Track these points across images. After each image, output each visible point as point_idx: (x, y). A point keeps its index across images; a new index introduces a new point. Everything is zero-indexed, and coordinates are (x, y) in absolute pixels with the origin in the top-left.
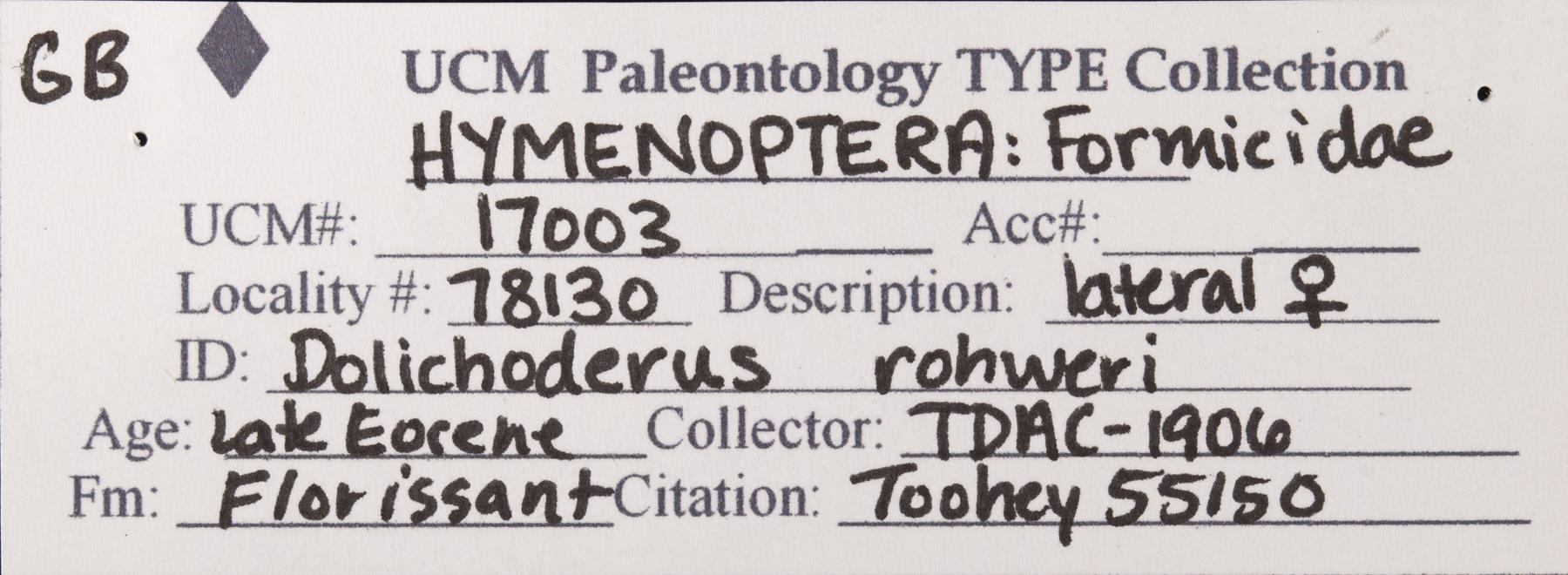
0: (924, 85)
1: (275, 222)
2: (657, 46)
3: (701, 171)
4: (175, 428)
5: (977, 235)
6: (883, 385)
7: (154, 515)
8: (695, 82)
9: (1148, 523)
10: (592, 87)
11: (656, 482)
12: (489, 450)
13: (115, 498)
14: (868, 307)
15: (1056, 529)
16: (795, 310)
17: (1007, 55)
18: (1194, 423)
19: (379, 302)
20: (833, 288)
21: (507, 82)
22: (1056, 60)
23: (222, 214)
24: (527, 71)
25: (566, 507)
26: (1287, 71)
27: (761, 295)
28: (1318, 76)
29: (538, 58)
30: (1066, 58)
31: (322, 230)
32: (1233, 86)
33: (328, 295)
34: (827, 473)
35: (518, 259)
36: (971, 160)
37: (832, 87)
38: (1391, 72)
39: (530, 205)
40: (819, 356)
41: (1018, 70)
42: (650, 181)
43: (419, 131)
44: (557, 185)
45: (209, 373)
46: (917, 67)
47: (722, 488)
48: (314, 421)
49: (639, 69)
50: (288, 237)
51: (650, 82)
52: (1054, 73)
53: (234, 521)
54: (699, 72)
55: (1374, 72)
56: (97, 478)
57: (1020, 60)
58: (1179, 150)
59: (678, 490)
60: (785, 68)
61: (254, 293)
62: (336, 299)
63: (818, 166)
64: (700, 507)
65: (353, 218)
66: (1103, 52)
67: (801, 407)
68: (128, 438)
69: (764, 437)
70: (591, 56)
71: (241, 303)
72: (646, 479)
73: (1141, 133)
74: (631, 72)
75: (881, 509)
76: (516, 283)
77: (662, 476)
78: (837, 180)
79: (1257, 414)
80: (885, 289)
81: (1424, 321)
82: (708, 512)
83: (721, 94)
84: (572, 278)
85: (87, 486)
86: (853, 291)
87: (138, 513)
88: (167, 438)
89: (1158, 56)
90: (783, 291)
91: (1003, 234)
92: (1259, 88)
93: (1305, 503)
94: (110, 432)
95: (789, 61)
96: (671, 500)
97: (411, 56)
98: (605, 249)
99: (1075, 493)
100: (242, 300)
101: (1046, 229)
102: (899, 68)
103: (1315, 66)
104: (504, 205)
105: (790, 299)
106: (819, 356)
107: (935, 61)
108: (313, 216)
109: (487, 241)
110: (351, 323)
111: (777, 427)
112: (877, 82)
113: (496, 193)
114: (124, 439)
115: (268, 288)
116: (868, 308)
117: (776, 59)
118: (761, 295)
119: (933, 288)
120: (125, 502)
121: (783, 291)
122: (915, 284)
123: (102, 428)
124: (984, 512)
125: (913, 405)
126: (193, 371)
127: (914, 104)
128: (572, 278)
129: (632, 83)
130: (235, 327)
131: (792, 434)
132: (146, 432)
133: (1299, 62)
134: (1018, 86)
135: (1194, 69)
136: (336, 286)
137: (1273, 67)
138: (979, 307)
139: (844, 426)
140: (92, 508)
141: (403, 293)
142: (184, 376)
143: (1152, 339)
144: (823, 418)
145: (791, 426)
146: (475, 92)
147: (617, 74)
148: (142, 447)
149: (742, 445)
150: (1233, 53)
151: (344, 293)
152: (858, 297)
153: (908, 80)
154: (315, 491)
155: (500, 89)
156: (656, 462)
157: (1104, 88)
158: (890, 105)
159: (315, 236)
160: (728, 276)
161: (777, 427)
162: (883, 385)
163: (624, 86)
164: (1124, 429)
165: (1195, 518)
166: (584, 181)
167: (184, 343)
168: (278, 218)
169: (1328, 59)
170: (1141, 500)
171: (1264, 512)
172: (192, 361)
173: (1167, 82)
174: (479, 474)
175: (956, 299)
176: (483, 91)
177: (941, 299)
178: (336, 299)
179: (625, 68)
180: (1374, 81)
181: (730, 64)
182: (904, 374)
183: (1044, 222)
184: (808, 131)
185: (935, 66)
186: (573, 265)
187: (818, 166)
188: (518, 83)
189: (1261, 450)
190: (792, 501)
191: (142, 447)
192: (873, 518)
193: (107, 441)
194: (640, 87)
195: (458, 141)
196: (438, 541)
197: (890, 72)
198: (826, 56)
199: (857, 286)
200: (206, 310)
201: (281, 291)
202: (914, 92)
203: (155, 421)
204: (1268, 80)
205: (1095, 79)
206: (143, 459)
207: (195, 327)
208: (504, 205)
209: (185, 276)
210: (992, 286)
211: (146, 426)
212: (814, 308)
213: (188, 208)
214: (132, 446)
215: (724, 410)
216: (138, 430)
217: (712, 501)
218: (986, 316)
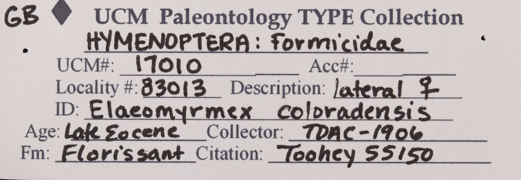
0: (286, 22)
4: (54, 131)
8: (201, 20)
10: (163, 22)
11: (210, 149)
13: (35, 153)
16: (255, 93)
17: (316, 11)
19: (121, 89)
20: (267, 86)
22: (335, 13)
24: (140, 16)
26: (419, 18)
27: (244, 88)
28: (430, 19)
29: (144, 11)
31: (103, 67)
32: (399, 23)
33: (105, 88)
34: (268, 148)
37: (252, 22)
38: (457, 18)
39: (154, 58)
40: (265, 107)
41: (320, 17)
44: (205, 54)
46: (283, 15)
47: (231, 151)
48: (96, 129)
49: (180, 15)
50: (92, 69)
51: (184, 20)
54: (203, 17)
56: (30, 147)
57: (321, 13)
59: (217, 151)
60: (235, 15)
63: (200, 47)
64: (224, 157)
66: (352, 11)
67: (256, 125)
69: (245, 134)
70: (163, 11)
71: (76, 90)
74: (177, 16)
78: (272, 53)
80: (284, 86)
82: (226, 159)
84: (194, 82)
85: (26, 149)
87: (43, 158)
88: (52, 134)
89: (372, 12)
90: (251, 87)
91: (322, 69)
93: (426, 156)
95: (236, 13)
96: (215, 155)
97: (98, 11)
99: (353, 152)
100: (77, 89)
101: (336, 68)
102: (277, 16)
105: (253, 90)
106: (265, 107)
109: (139, 69)
110: (112, 97)
114: (38, 134)
116: (278, 93)
117: (231, 12)
118: (244, 88)
120: (39, 154)
121: (251, 87)
122: (294, 85)
125: (305, 125)
126: (61, 112)
127: (282, 29)
128: (194, 82)
129: (178, 21)
131: (254, 133)
133: (424, 14)
134: (320, 22)
136: (107, 85)
137: (414, 16)
140: (28, 156)
142: (58, 114)
144: (264, 128)
146: (122, 23)
147: (173, 17)
149: (237, 137)
150: (399, 11)
151: (110, 88)
152: (275, 89)
153: (280, 20)
154: (95, 152)
155: (130, 23)
156: (210, 142)
157: (352, 23)
159: (100, 69)
161: (249, 131)
163: (175, 22)
164: (367, 132)
167: (58, 103)
169: (434, 13)
172: (60, 109)
176: (124, 23)
177: (301, 90)
179: (175, 15)
183: (335, 66)
184: (197, 38)
185: (290, 15)
186: (195, 78)
187: (200, 47)
188: (136, 21)
190: (254, 155)
194: (181, 22)
197: (274, 17)
198: (249, 11)
199: (275, 86)
200: (65, 93)
201: (89, 86)
202: (282, 24)
204: (412, 21)
205: (349, 20)
206: (44, 140)
207: (62, 98)
208: (146, 59)
209: (58, 81)
210: (318, 86)
211: (45, 130)
213: (59, 60)
214: (41, 136)
215: (232, 126)
216: (43, 131)
217: (227, 155)
218: (317, 96)
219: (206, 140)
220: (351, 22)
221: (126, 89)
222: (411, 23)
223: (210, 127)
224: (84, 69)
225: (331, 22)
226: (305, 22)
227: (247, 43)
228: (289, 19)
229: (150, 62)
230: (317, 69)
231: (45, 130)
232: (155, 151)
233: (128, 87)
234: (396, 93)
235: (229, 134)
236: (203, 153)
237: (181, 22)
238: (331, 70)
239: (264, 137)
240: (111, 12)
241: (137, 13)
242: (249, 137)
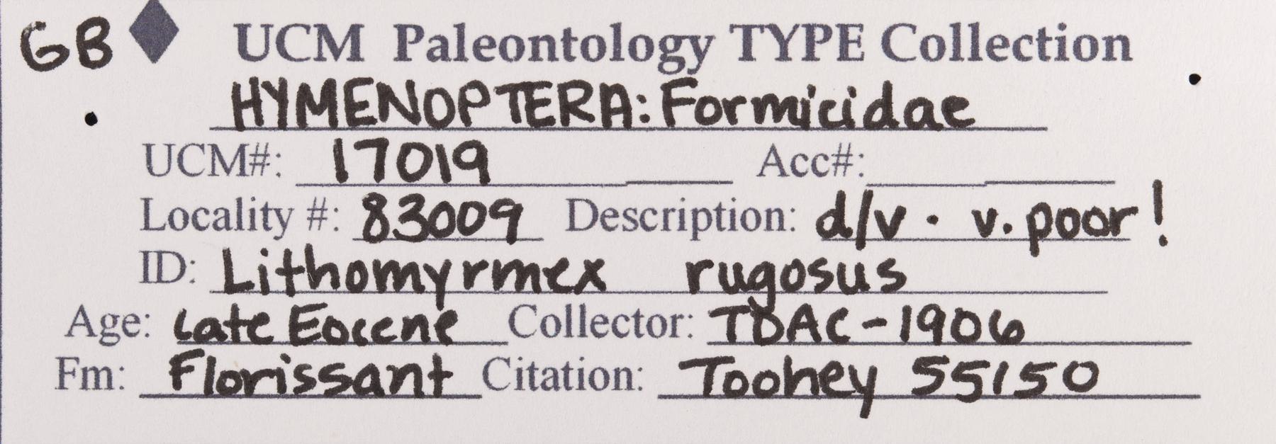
0: (700, 55)
3: (423, 123)
5: (768, 170)
6: (694, 287)
8: (495, 52)
10: (402, 56)
11: (515, 364)
13: (91, 375)
16: (625, 229)
17: (774, 29)
18: (940, 316)
19: (298, 221)
20: (655, 212)
22: (819, 34)
24: (344, 43)
25: (428, 386)
28: (1052, 48)
29: (355, 31)
30: (828, 31)
32: (975, 57)
36: (617, 120)
37: (617, 57)
38: (1118, 46)
40: (644, 266)
41: (783, 43)
43: (237, 88)
46: (694, 40)
47: (567, 369)
50: (228, 171)
51: (453, 52)
55: (528, 46)
56: (77, 359)
58: (769, 111)
59: (532, 369)
60: (576, 39)
61: (201, 214)
62: (265, 220)
63: (516, 118)
64: (550, 383)
66: (861, 27)
67: (628, 305)
69: (600, 329)
70: (402, 29)
72: (507, 361)
73: (741, 100)
77: (520, 359)
79: (996, 315)
80: (695, 212)
81: (653, 293)
82: (556, 388)
85: (69, 366)
88: (131, 328)
89: (910, 30)
91: (788, 169)
94: (87, 324)
95: (579, 33)
96: (527, 378)
97: (242, 29)
99: (873, 372)
100: (191, 219)
101: (822, 166)
102: (678, 40)
103: (1050, 39)
105: (621, 221)
106: (644, 266)
110: (276, 238)
114: (97, 328)
115: (211, 212)
116: (682, 228)
117: (567, 32)
119: (733, 212)
122: (719, 210)
123: (81, 320)
126: (153, 275)
127: (690, 72)
129: (437, 53)
131: (623, 326)
132: (115, 323)
133: (1035, 36)
134: (784, 56)
135: (601, 41)
140: (73, 383)
141: (317, 214)
142: (146, 279)
144: (647, 314)
145: (621, 320)
146: (301, 60)
147: (424, 45)
148: (112, 335)
149: (583, 334)
150: (975, 28)
151: (272, 216)
152: (674, 219)
153: (686, 50)
155: (320, 58)
156: (516, 347)
159: (248, 169)
160: (572, 202)
161: (611, 321)
162: (694, 287)
163: (431, 56)
164: (881, 322)
167: (146, 254)
168: (219, 153)
169: (1060, 34)
170: (1043, 383)
172: (152, 269)
174: (400, 355)
177: (739, 221)
178: (265, 220)
179: (430, 40)
180: (528, 52)
182: (709, 279)
183: (820, 160)
185: (710, 38)
188: (336, 53)
189: (1003, 340)
190: (621, 379)
191: (112, 335)
193: (84, 330)
194: (445, 57)
195: (264, 94)
197: (670, 44)
199: (673, 210)
200: (163, 228)
201: (222, 213)
202: (691, 61)
203: (122, 312)
205: (853, 51)
206: (113, 344)
207: (154, 241)
208: (360, 145)
209: (147, 201)
210: (779, 211)
211: (115, 318)
213: (149, 147)
215: (569, 308)
216: (109, 321)
217: (559, 379)
219: (505, 343)
220: (859, 56)
221: (311, 219)
223: (516, 309)
225: (810, 56)
226: (747, 56)
228: (708, 46)
229: (372, 152)
231: (115, 318)
232: (371, 370)
233: (317, 214)
235: (562, 326)
236: (501, 374)
237: (445, 57)
238: (810, 172)
239: (647, 335)
240: (274, 34)
241: (339, 35)
242: (611, 334)
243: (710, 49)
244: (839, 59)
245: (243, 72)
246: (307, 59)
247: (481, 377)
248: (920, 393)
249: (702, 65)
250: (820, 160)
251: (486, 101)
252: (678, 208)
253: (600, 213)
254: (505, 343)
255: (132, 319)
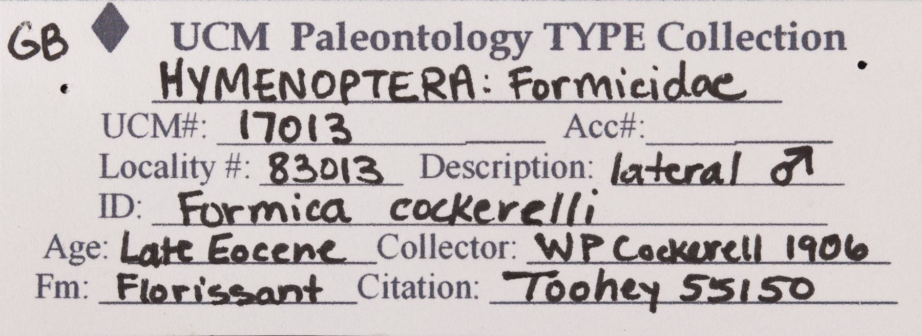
0: (522, 46)
1: (157, 124)
2: (341, 20)
4: (98, 246)
7: (86, 297)
8: (367, 43)
9: (735, 303)
10: (298, 46)
11: (382, 279)
12: (292, 260)
13: (63, 287)
14: (508, 175)
15: (648, 306)
16: (465, 177)
19: (219, 171)
20: (487, 164)
21: (241, 44)
22: (611, 30)
23: (126, 120)
24: (254, 37)
27: (444, 168)
28: (786, 41)
31: (185, 129)
32: (728, 47)
33: (189, 167)
35: (284, 146)
36: (462, 90)
37: (459, 47)
38: (835, 39)
42: (379, 102)
45: (119, 213)
46: (517, 35)
47: (421, 282)
49: (329, 35)
50: (166, 134)
51: (336, 44)
52: (609, 40)
53: (318, 300)
56: (52, 276)
57: (586, 30)
59: (395, 282)
60: (428, 34)
61: (145, 166)
64: (408, 293)
65: (642, 122)
66: (642, 25)
68: (71, 252)
69: (446, 252)
70: (297, 26)
71: (137, 172)
72: (377, 276)
74: (324, 37)
75: (529, 296)
76: (278, 160)
78: (313, 102)
80: (518, 164)
82: (413, 296)
83: (445, 51)
86: (499, 166)
87: (76, 296)
88: (94, 252)
89: (679, 27)
91: (587, 132)
92: (362, 49)
95: (431, 29)
96: (391, 289)
97: (177, 27)
98: (290, 141)
100: (137, 170)
101: (612, 129)
102: (505, 34)
103: (784, 33)
104: (257, 115)
105: (462, 170)
107: (528, 30)
108: (180, 121)
109: (245, 135)
111: (454, 246)
112: (489, 43)
113: (252, 108)
114: (68, 252)
115: (154, 163)
117: (422, 28)
118: (444, 168)
120: (68, 290)
122: (535, 162)
124: (599, 295)
126: (109, 212)
127: (515, 58)
129: (324, 44)
130: (134, 186)
131: (463, 250)
132: (81, 248)
133: (774, 31)
134: (584, 47)
136: (194, 162)
137: (370, 35)
138: (573, 176)
139: (493, 245)
140: (49, 293)
141: (233, 166)
142: (104, 215)
143: (297, 196)
147: (314, 38)
149: (433, 256)
150: (728, 25)
151: (199, 167)
152: (501, 169)
153: (511, 43)
155: (236, 48)
156: (383, 266)
157: (643, 49)
158: (499, 59)
159: (181, 132)
160: (425, 156)
161: (454, 246)
163: (319, 46)
165: (563, 300)
166: (662, 102)
167: (104, 196)
168: (160, 123)
169: (792, 30)
170: (698, 290)
171: (698, 297)
172: (108, 206)
173: (685, 45)
175: (559, 168)
177: (550, 171)
179: (319, 35)
181: (390, 33)
183: (611, 126)
185: (529, 33)
188: (248, 44)
190: (463, 290)
192: (525, 300)
193: (58, 253)
194: (330, 47)
196: (567, 311)
197: (499, 38)
198: (710, 27)
199: (501, 163)
200: (116, 176)
201: (161, 165)
202: (515, 51)
203: (87, 241)
205: (637, 43)
206: (79, 264)
207: (109, 186)
208: (257, 115)
209: (104, 156)
212: (476, 175)
213: (106, 116)
214: (72, 256)
215: (422, 236)
216: (76, 247)
217: (415, 290)
221: (229, 169)
222: (750, 49)
224: (152, 133)
225: (604, 46)
226: (557, 46)
227: (468, 81)
229: (265, 121)
230: (578, 132)
234: (726, 174)
235: (418, 250)
236: (371, 286)
237: (330, 47)
241: (250, 31)
242: (454, 256)
243: (528, 42)
244: (626, 49)
245: (172, 56)
246: (227, 49)
247: (357, 289)
248: (685, 299)
249: (523, 54)
250: (611, 126)
251: (357, 81)
252: (504, 161)
253: (446, 164)
254: (375, 263)
255: (93, 245)
